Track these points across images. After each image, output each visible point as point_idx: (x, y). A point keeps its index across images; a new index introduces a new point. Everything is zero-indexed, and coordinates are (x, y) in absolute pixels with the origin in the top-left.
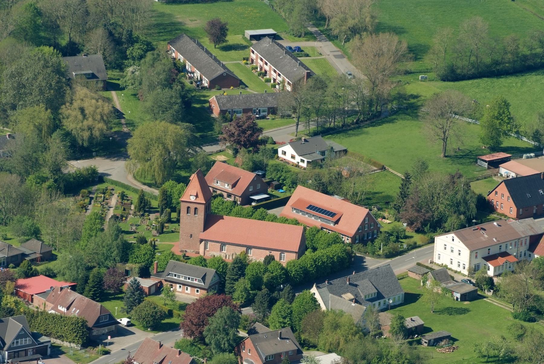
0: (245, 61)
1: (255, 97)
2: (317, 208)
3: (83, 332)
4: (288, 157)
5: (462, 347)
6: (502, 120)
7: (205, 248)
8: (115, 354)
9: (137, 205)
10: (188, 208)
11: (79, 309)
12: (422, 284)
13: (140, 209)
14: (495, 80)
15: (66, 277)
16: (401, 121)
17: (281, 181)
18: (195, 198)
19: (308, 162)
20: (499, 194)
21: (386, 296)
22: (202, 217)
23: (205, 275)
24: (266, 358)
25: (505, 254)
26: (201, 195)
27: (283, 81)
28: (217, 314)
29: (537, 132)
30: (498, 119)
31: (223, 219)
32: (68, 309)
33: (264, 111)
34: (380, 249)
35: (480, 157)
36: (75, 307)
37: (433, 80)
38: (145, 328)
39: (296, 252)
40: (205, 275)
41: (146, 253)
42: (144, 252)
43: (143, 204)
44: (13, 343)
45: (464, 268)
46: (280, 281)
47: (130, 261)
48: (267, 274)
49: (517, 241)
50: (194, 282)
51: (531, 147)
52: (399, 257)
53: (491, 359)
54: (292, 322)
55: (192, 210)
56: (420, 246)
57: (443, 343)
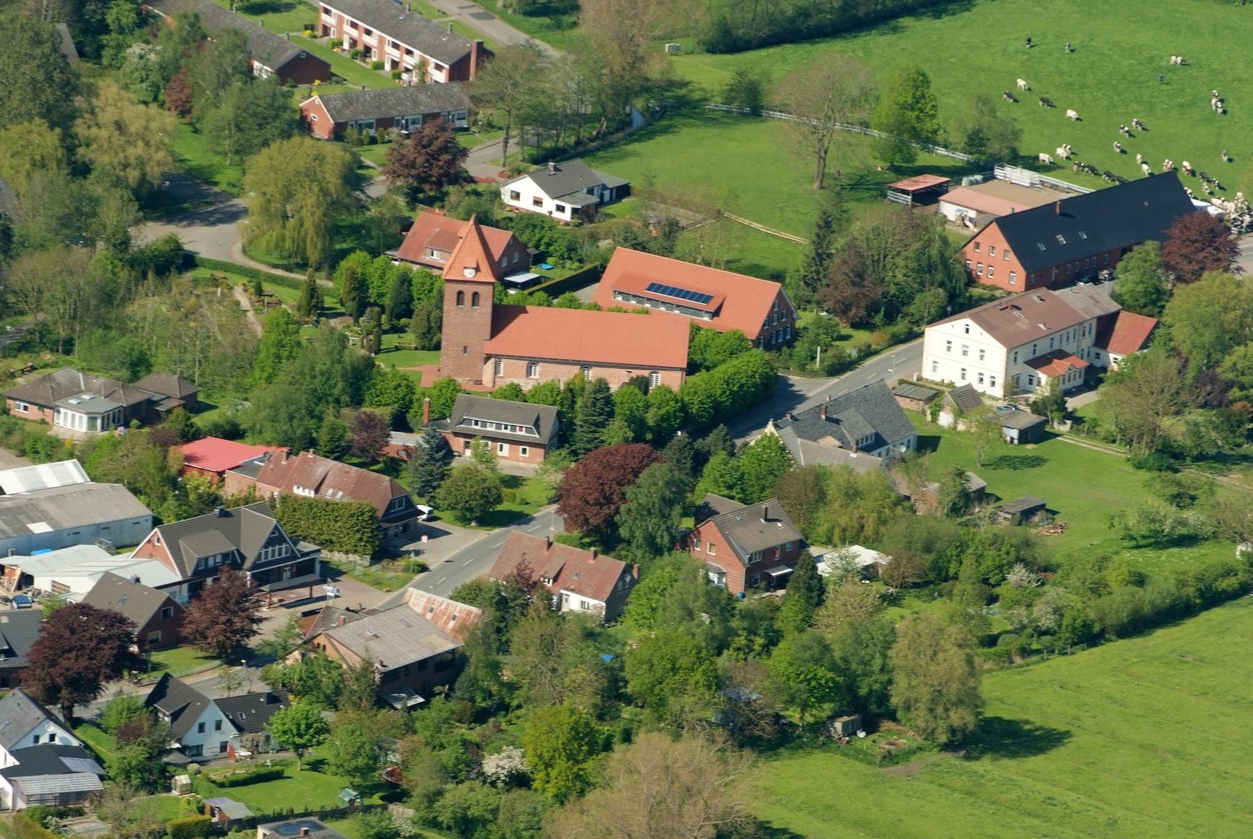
0: (309, 32)
1: (393, 94)
2: (661, 286)
3: (372, 531)
4: (526, 204)
5: (1073, 524)
6: (922, 111)
7: (496, 372)
8: (440, 569)
9: (304, 303)
10: (460, 293)
11: (341, 490)
12: (929, 418)
13: (310, 310)
14: (807, 47)
15: (267, 435)
16: (685, 131)
17: (542, 248)
18: (473, 272)
19: (574, 211)
20: (984, 247)
21: (889, 441)
22: (489, 310)
23: (538, 419)
24: (750, 559)
25: (1061, 355)
26: (485, 267)
27: (422, 65)
28: (643, 477)
29: (977, 133)
30: (913, 109)
31: (526, 312)
32: (317, 491)
33: (414, 122)
34: (813, 358)
35: (893, 185)
36: (332, 487)
37: (692, 53)
38: (464, 520)
39: (682, 369)
40: (538, 419)
41: (399, 385)
42: (395, 383)
43: (314, 300)
44: (260, 555)
45: (993, 384)
46: (675, 423)
47: (367, 403)
48: (652, 411)
49: (1076, 327)
50: (518, 433)
51: (960, 164)
52: (849, 374)
53: (1142, 542)
54: (746, 495)
55: (468, 298)
56: (876, 352)
57: (1036, 519)
